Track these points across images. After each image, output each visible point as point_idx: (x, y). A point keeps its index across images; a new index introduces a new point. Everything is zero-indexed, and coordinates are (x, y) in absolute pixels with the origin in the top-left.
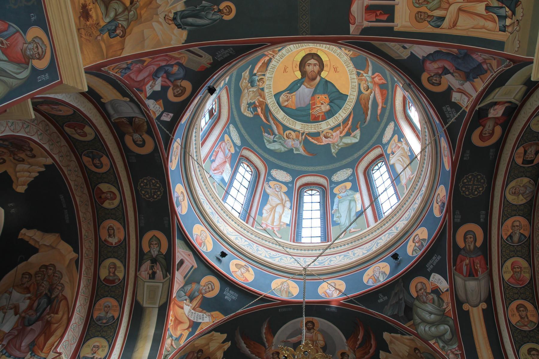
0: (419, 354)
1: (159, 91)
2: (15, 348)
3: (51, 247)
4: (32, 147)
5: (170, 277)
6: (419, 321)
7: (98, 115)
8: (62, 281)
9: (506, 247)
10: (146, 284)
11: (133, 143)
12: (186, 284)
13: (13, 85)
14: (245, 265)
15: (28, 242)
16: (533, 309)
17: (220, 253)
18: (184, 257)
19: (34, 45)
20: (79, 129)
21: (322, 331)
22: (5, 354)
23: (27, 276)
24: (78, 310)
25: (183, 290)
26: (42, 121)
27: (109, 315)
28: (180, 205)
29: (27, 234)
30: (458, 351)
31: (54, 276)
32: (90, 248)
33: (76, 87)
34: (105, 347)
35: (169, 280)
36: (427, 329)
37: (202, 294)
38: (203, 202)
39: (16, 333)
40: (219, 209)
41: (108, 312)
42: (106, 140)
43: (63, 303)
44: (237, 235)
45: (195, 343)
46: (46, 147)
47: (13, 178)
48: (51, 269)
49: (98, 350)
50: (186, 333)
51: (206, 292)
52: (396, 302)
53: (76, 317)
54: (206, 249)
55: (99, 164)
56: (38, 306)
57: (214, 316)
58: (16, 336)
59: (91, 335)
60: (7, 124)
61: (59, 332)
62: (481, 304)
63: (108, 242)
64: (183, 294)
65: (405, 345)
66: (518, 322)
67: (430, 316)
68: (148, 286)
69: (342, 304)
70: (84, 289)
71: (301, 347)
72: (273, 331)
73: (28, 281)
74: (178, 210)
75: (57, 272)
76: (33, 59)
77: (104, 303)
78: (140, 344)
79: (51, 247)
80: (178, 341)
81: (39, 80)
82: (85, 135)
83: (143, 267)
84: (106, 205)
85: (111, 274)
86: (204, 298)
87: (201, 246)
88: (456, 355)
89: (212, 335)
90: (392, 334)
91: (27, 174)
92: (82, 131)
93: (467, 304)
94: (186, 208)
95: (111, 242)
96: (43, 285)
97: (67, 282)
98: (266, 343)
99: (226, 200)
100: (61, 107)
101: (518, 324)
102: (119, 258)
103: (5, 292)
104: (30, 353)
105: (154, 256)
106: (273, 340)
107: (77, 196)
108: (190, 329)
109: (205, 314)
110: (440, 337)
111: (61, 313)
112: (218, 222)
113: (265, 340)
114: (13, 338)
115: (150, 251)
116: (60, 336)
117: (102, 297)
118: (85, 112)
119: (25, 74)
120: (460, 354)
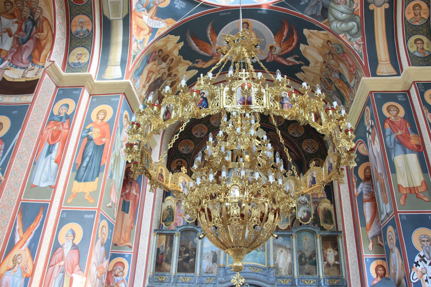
0: (330, 45)
2: (19, 61)
6: (332, 19)
9: (409, 26)
16: (426, 8)
21: (255, 30)
24: (58, 27)
27: (85, 29)
30: (361, 42)
34: (87, 54)
36: (338, 25)
37: (156, 5)
39: (16, 50)
43: (45, 23)
49: (81, 56)
50: (148, 37)
51: (159, 3)
52: (315, 4)
53: (58, 34)
56: (26, 28)
57: (168, 22)
58: (16, 53)
59: (73, 46)
61: (48, 46)
62: (385, 4)
64: (141, 6)
65: (320, 38)
66: (412, 18)
67: (342, 15)
69: (271, 7)
70: (59, 10)
71: (239, 34)
72: (216, 32)
73: (11, 8)
80: (142, 44)
86: (158, 9)
88: (359, 45)
89: (168, 38)
90: (311, 30)
93: (373, 5)
96: (25, 10)
98: (211, 41)
101: (411, 20)
106: (216, 38)
108: (151, 34)
110: (348, 32)
111: (45, 31)
113: (210, 39)
120: (362, 44)
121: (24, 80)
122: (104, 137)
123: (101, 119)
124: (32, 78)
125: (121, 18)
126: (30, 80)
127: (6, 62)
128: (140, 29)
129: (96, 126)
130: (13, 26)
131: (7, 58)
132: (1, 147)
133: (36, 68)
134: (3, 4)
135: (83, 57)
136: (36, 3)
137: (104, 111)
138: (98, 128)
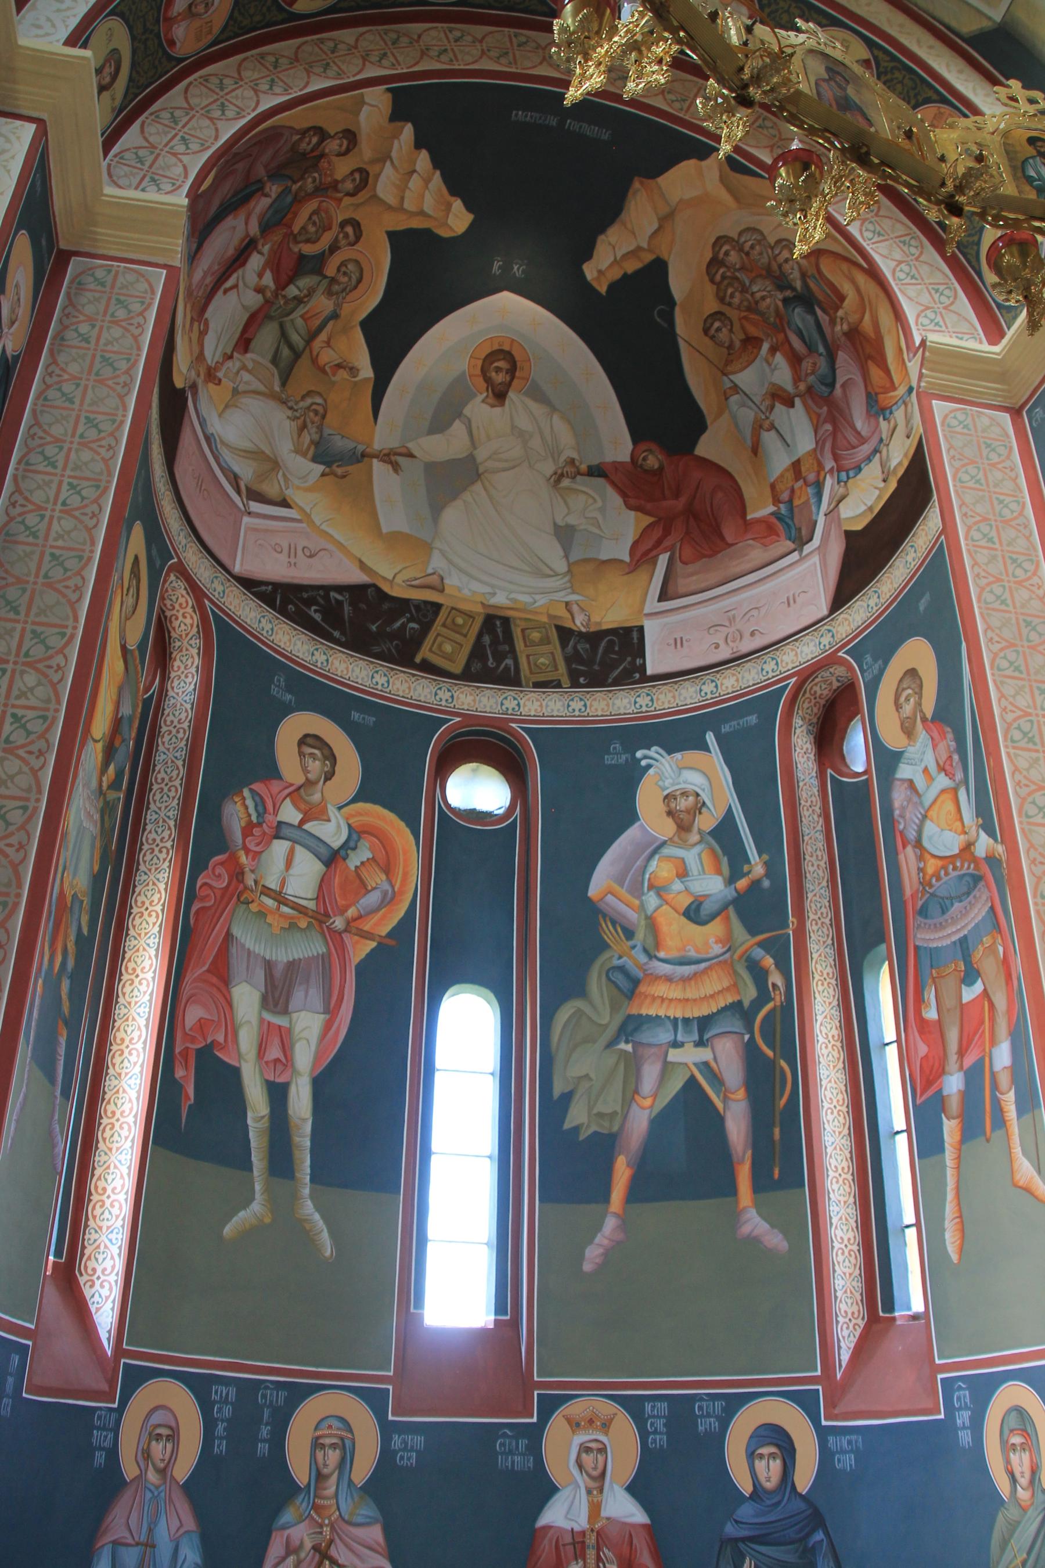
3: (666, 219)
22: (848, 478)
23: (717, 324)
29: (604, 265)
31: (747, 254)
39: (828, 427)
43: (827, 268)
47: (416, 224)
48: (727, 254)
58: (836, 429)
61: (886, 318)
73: (731, 331)
75: (743, 239)
79: (666, 219)
91: (415, 182)
96: (758, 295)
103: (727, 399)
104: (881, 419)
111: (847, 288)
116: (894, 323)
121: (893, 485)
124: (906, 455)
126: (906, 464)
127: (829, 482)
130: (775, 369)
131: (823, 469)
132: (949, 746)
133: (899, 414)
134: (707, 340)
136: (759, 242)
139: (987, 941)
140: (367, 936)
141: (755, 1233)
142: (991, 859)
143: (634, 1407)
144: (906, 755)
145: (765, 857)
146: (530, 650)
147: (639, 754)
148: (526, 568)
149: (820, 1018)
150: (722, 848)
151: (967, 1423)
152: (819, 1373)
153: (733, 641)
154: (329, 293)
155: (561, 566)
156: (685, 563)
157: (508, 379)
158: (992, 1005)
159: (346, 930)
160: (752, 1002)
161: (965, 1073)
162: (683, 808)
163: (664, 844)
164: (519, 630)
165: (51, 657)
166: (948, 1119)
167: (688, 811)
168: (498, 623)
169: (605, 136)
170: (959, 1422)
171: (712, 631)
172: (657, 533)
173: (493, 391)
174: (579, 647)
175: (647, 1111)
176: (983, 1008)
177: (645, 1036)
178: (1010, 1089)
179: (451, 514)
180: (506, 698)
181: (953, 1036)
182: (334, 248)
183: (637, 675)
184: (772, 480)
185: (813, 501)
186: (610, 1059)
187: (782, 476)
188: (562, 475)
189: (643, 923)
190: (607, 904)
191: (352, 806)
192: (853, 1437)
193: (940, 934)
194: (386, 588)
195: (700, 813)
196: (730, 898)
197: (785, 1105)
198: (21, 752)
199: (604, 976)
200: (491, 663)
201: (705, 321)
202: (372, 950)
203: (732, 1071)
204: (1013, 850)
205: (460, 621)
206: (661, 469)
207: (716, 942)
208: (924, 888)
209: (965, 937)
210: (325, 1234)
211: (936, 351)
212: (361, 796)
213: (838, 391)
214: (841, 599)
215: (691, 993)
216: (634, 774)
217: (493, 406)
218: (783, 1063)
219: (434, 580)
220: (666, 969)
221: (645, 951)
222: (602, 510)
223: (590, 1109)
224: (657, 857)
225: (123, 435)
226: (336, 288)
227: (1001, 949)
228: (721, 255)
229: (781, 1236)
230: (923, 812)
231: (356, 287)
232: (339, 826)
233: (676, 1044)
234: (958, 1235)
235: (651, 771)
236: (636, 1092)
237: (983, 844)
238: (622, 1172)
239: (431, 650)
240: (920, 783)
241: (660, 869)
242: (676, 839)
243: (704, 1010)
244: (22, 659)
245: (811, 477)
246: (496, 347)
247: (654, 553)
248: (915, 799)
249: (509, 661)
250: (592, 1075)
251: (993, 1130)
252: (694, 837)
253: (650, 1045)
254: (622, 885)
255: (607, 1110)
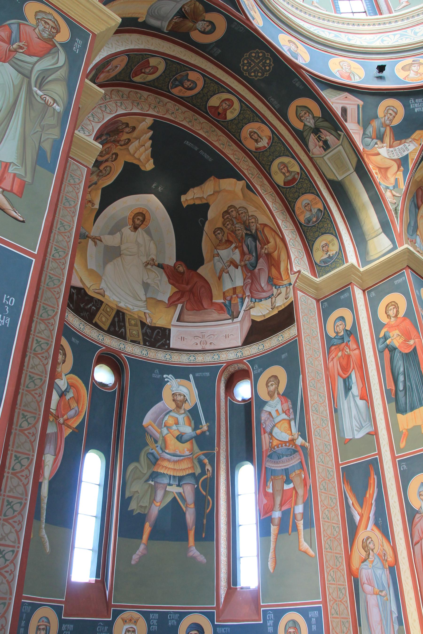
1: (60, 342)
4: (125, 122)
5: (343, 134)
7: (149, 38)
8: (250, 214)
10: (325, 158)
11: (203, 34)
12: (365, 128)
13: (64, 76)
14: (413, 61)
15: (194, 204)
17: (376, 71)
18: (342, 103)
19: (42, 23)
20: (146, 68)
23: (219, 232)
25: (366, 136)
26: (111, 92)
27: (314, 211)
28: (298, 55)
31: (239, 214)
32: (250, 167)
33: (109, 27)
35: (345, 138)
37: (389, 126)
38: (318, 32)
39: (250, 281)
40: (340, 26)
41: (311, 209)
42: (177, 56)
43: (266, 230)
44: (381, 37)
45: (416, 177)
46: (135, 111)
48: (232, 211)
49: (328, 247)
50: (400, 175)
51: (391, 121)
53: (287, 234)
54: (358, 78)
55: (190, 84)
57: (417, 139)
59: (312, 239)
60: (90, 120)
61: (283, 256)
63: (260, 148)
64: (370, 140)
68: (328, 159)
73: (223, 235)
74: (300, 62)
75: (239, 209)
76: (54, 37)
77: (302, 204)
78: (362, 216)
79: (216, 193)
80: (397, 187)
81: (7, 296)
82: (156, 69)
83: (311, 145)
84: (230, 116)
85: (287, 174)
87: (351, 80)
91: (142, 149)
92: (150, 68)
94: (306, 53)
95: (263, 145)
96: (237, 228)
97: (255, 211)
99: (340, 11)
100: (114, 63)
102: (282, 154)
103: (214, 257)
104: (274, 287)
105: (313, 126)
107: (199, 130)
108: (402, 168)
109: (405, 144)
111: (271, 240)
112: (349, 40)
114: (251, 286)
115: (305, 125)
117: (295, 200)
118: (137, 47)
119: (62, 57)
121: (276, 312)
122: (410, 339)
123: (394, 315)
125: (352, 170)
126: (283, 307)
127: (247, 300)
128: (384, 170)
129: (392, 327)
130: (235, 254)
134: (214, 235)
135: (331, 247)
136: (245, 213)
137: (393, 304)
138: (396, 330)
139: (297, 472)
140: (69, 427)
141: (194, 555)
142: (302, 447)
143: (146, 615)
144: (269, 403)
145: (208, 424)
146: (130, 327)
147: (165, 376)
148: (132, 295)
149: (222, 483)
150: (192, 416)
151: (272, 624)
152: (215, 606)
153: (203, 344)
154: (98, 175)
155: (144, 298)
156: (188, 310)
157: (141, 223)
158: (296, 492)
159: (63, 424)
160: (199, 474)
161: (282, 512)
162: (179, 400)
163: (171, 411)
164: (127, 319)
165: (49, 319)
166: (273, 525)
167: (181, 401)
168: (121, 314)
169: (210, 160)
170: (268, 624)
171: (195, 338)
172: (178, 296)
173: (134, 226)
174: (148, 331)
175: (158, 507)
176: (293, 492)
177: (159, 480)
178: (301, 520)
179: (109, 267)
180: (121, 344)
181: (278, 500)
182: (106, 161)
183: (167, 347)
184: (224, 291)
185: (239, 304)
186: (146, 487)
187: (228, 290)
188: (148, 264)
189: (161, 438)
190: (149, 429)
191: (69, 375)
192: (227, 629)
193: (277, 465)
194: (87, 291)
195: (185, 403)
196: (193, 435)
197: (209, 512)
198: (39, 356)
199: (146, 456)
200: (117, 329)
201: (215, 229)
202: (71, 433)
203: (190, 497)
204: (312, 446)
205: (108, 310)
206: (183, 273)
207: (187, 450)
208: (271, 449)
209: (288, 469)
210: (48, 544)
211: (303, 276)
212: (72, 372)
213: (256, 270)
214: (247, 341)
215: (177, 467)
216: (162, 383)
217: (132, 231)
218: (209, 497)
219: (101, 291)
220: (168, 457)
221: (161, 449)
222: (160, 281)
223: (138, 504)
224: (168, 415)
225: (73, 233)
226: (101, 174)
227: (303, 476)
228: (230, 211)
229: (204, 557)
230: (274, 424)
231: (106, 176)
232: (65, 382)
233: (170, 485)
234: (274, 563)
235: (168, 383)
236: (154, 500)
237: (300, 441)
238: (147, 528)
239: (98, 319)
240: (274, 414)
241: (169, 420)
242: (175, 410)
243: (181, 474)
244: (39, 317)
245: (240, 295)
246: (141, 211)
247: (176, 303)
248: (271, 419)
249: (123, 330)
250: (139, 492)
251: (292, 531)
252: (182, 411)
253: (160, 483)
254: (155, 423)
255: (144, 505)
